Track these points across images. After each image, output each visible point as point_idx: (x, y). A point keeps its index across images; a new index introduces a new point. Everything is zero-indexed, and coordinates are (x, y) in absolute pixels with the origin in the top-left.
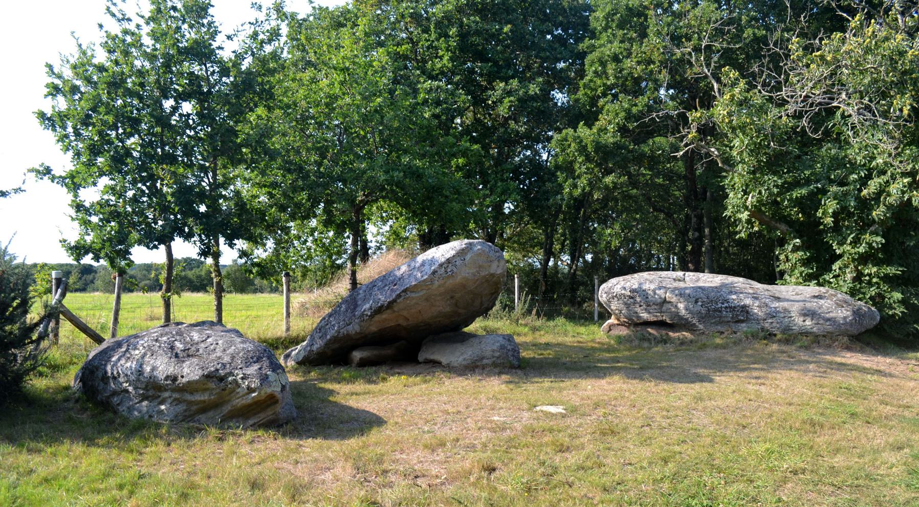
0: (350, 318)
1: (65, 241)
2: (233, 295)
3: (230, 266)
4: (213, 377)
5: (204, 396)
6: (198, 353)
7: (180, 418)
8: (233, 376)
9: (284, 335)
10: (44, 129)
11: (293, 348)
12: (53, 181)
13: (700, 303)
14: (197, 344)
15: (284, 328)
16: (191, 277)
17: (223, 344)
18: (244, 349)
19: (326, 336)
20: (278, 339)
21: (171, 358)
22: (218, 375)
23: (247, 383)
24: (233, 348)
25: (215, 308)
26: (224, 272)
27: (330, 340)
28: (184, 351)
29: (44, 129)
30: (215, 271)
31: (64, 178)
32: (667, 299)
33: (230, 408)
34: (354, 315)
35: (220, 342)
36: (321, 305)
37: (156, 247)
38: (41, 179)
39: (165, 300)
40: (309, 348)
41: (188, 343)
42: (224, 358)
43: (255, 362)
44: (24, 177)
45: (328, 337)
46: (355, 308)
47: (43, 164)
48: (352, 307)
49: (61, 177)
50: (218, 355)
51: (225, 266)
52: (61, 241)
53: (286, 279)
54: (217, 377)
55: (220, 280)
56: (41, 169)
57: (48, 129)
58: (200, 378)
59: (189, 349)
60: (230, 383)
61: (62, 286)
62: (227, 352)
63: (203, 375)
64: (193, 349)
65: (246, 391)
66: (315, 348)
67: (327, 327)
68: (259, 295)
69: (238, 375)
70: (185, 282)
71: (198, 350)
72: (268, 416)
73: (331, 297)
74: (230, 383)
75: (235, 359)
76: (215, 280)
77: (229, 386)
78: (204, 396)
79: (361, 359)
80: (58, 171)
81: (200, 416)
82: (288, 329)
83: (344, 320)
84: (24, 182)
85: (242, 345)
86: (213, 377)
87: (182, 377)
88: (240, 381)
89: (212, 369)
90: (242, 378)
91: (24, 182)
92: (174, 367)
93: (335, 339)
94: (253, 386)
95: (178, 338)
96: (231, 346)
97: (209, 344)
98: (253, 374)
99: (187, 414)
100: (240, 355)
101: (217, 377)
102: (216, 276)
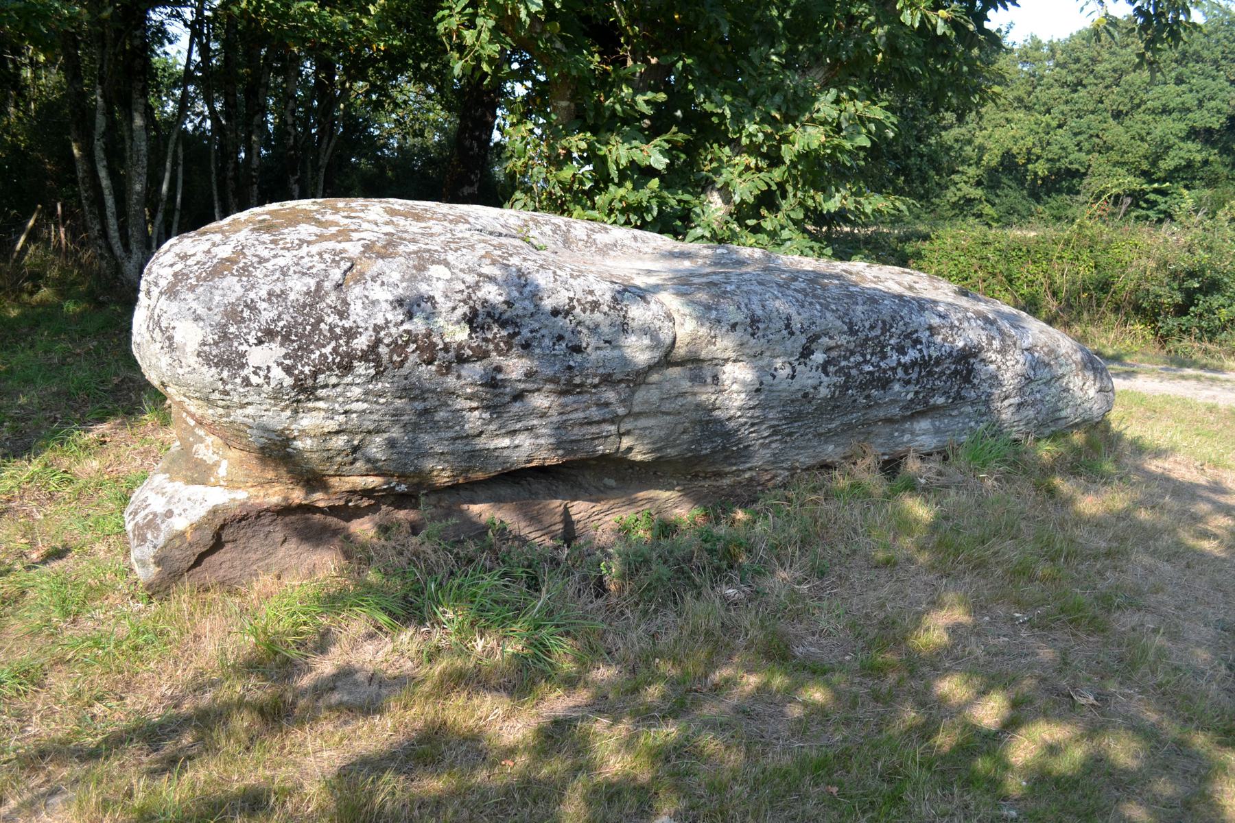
13: (819, 357)
32: (681, 351)
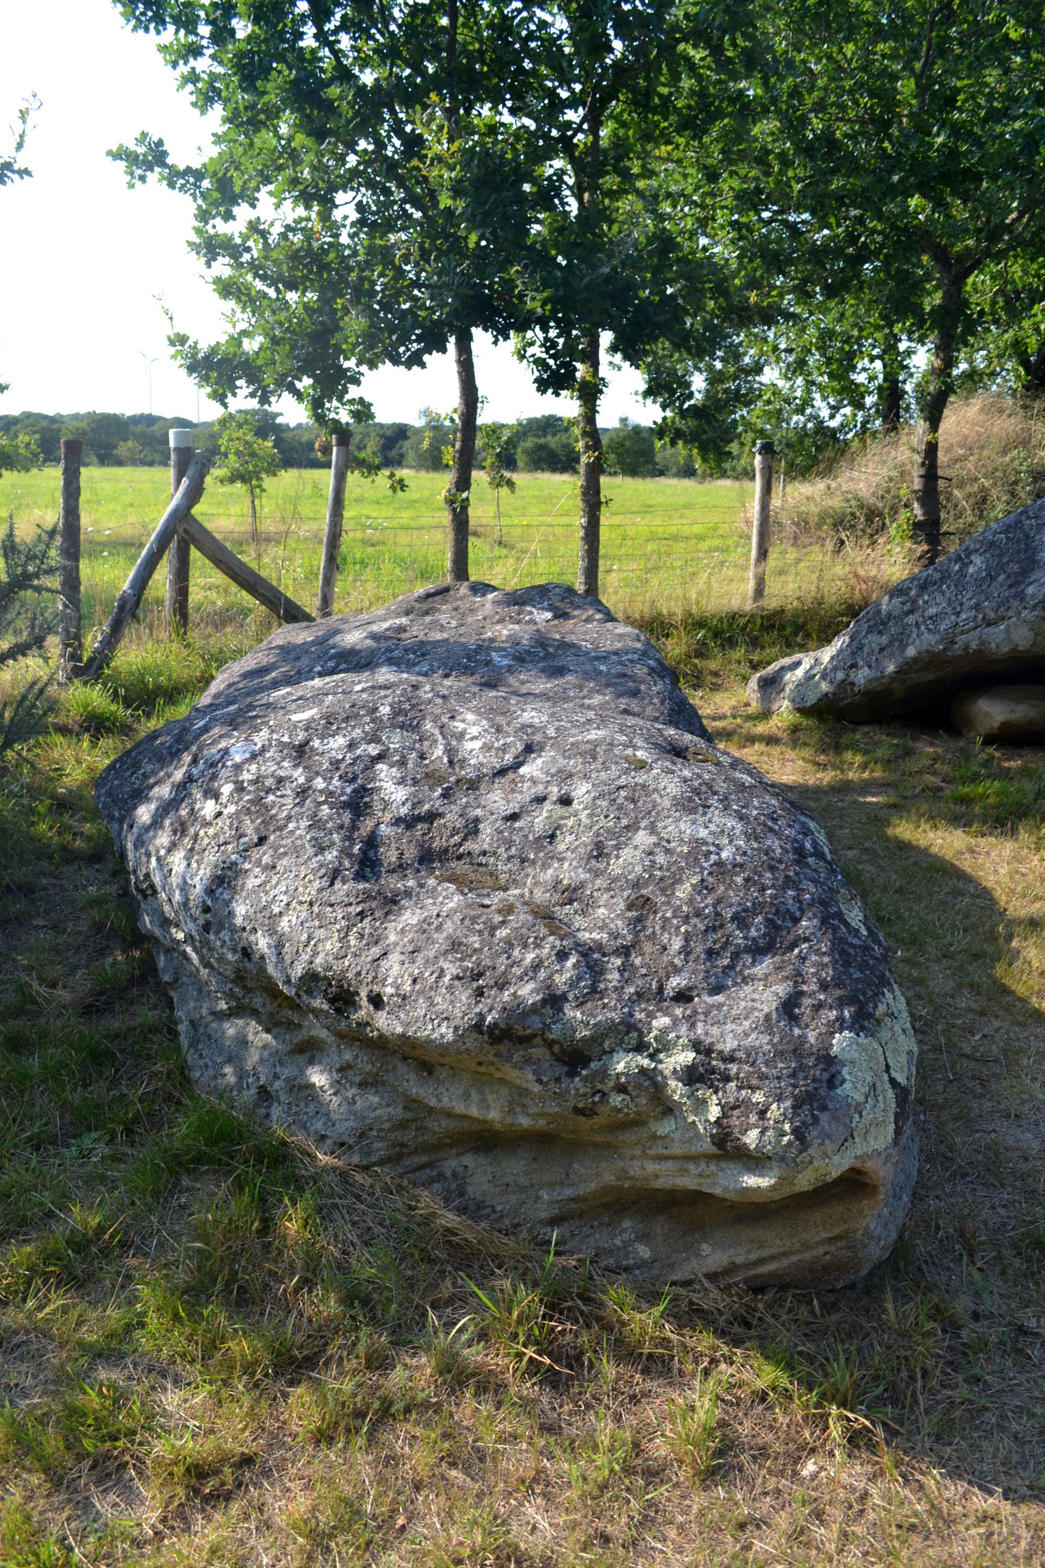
0: (1004, 603)
1: (182, 340)
2: (619, 480)
3: (615, 429)
4: (525, 1040)
5: (485, 1105)
6: (469, 846)
7: (380, 1148)
8: (640, 1047)
9: (749, 606)
10: (135, 29)
11: (786, 661)
12: (172, 185)
14: (473, 785)
15: (751, 586)
16: (554, 446)
17: (592, 806)
18: (698, 850)
19: (903, 647)
20: (733, 616)
21: (334, 875)
22: (556, 1031)
23: (714, 1112)
24: (643, 838)
25: (582, 533)
26: (605, 441)
27: (915, 660)
28: (408, 823)
29: (135, 29)
30: (585, 434)
31: (199, 175)
33: (609, 1178)
34: (1021, 596)
35: (581, 791)
36: (813, 520)
37: (416, 360)
38: (143, 178)
39: (454, 510)
40: (840, 676)
41: (432, 778)
42: (588, 907)
43: (758, 950)
44: (19, 127)
45: (911, 652)
46: (1025, 573)
47: (144, 135)
48: (1015, 568)
49: (189, 170)
50: (570, 872)
51: (606, 430)
52: (172, 343)
53: (764, 461)
54: (549, 1044)
55: (598, 458)
56: (141, 150)
57: (147, 30)
58: (460, 1038)
59: (432, 817)
60: (622, 1089)
61: (190, 471)
62: (616, 867)
63: (478, 1027)
64: (452, 817)
65: (707, 1146)
66: (862, 676)
67: (911, 619)
68: (663, 481)
69: (665, 1046)
70: (544, 455)
71: (472, 829)
72: (806, 1247)
73: (836, 503)
74: (622, 1089)
75: (654, 923)
76: (584, 459)
77: (617, 1100)
78: (628, 1065)
79: (1004, 725)
80: (179, 157)
81: (468, 1160)
82: (759, 592)
83: (977, 607)
84: (20, 146)
85: (686, 827)
86: (525, 1040)
87: (377, 1001)
88: (677, 1089)
89: (528, 992)
90: (692, 1076)
91: (20, 146)
92: (344, 939)
93: (929, 660)
94: (751, 1138)
95: (395, 740)
96: (632, 828)
97: (527, 792)
98: (751, 1055)
99: (408, 1137)
100: (683, 891)
101: (549, 1044)
102: (587, 447)
